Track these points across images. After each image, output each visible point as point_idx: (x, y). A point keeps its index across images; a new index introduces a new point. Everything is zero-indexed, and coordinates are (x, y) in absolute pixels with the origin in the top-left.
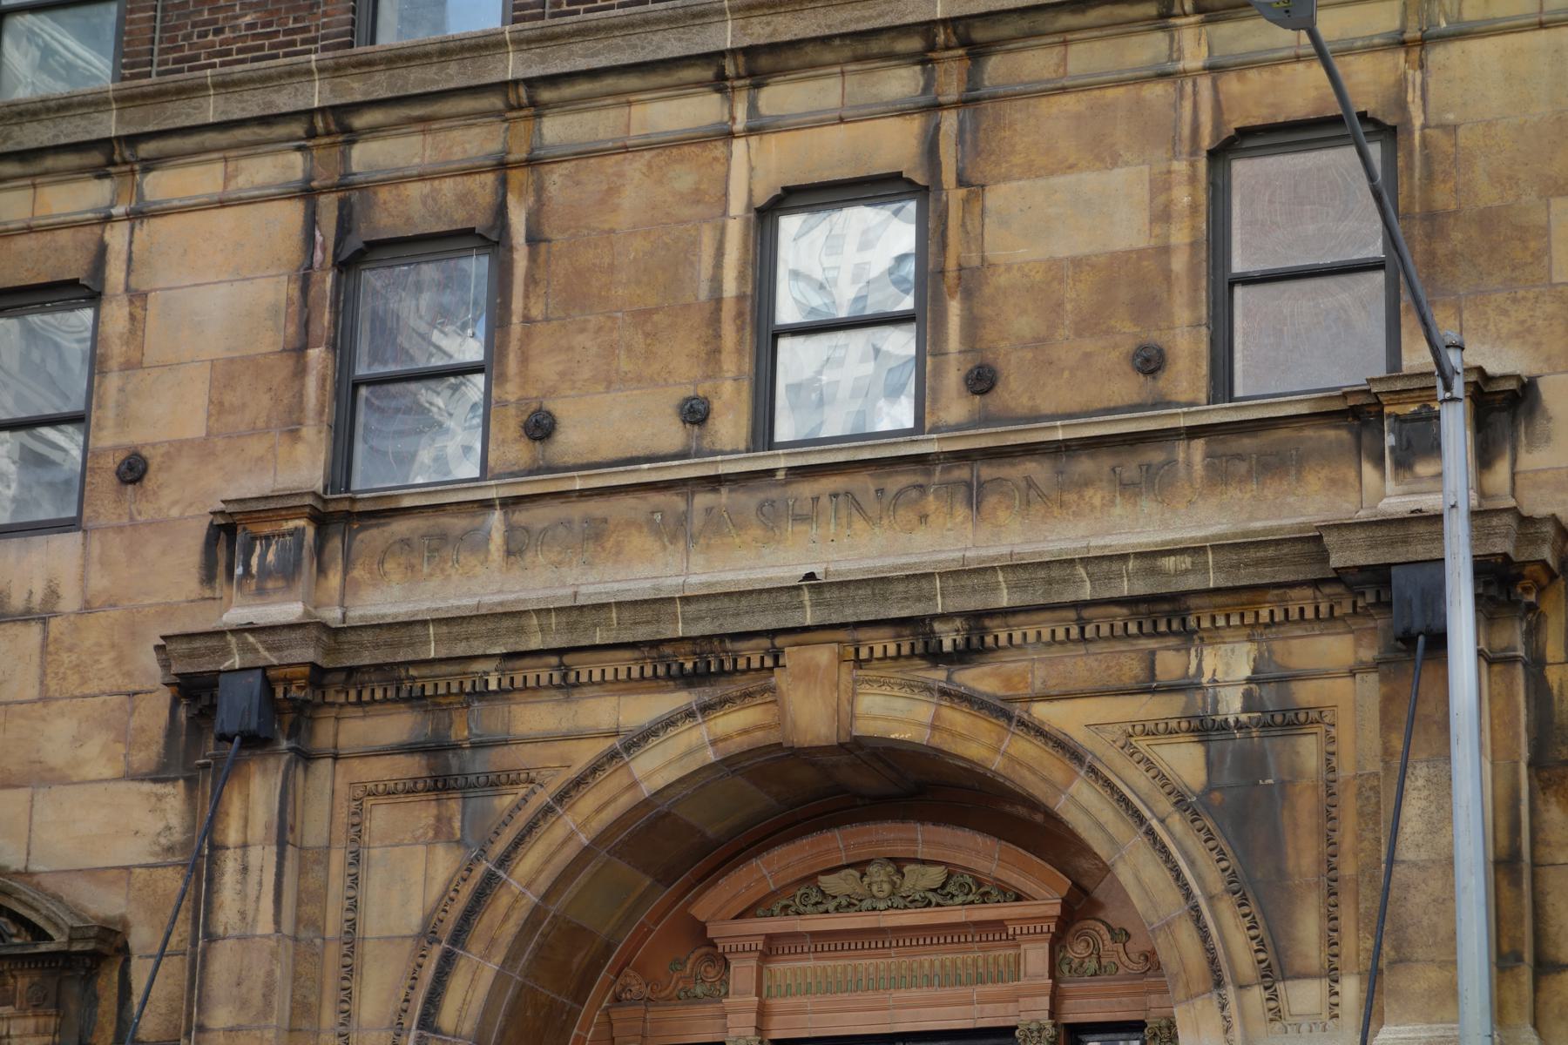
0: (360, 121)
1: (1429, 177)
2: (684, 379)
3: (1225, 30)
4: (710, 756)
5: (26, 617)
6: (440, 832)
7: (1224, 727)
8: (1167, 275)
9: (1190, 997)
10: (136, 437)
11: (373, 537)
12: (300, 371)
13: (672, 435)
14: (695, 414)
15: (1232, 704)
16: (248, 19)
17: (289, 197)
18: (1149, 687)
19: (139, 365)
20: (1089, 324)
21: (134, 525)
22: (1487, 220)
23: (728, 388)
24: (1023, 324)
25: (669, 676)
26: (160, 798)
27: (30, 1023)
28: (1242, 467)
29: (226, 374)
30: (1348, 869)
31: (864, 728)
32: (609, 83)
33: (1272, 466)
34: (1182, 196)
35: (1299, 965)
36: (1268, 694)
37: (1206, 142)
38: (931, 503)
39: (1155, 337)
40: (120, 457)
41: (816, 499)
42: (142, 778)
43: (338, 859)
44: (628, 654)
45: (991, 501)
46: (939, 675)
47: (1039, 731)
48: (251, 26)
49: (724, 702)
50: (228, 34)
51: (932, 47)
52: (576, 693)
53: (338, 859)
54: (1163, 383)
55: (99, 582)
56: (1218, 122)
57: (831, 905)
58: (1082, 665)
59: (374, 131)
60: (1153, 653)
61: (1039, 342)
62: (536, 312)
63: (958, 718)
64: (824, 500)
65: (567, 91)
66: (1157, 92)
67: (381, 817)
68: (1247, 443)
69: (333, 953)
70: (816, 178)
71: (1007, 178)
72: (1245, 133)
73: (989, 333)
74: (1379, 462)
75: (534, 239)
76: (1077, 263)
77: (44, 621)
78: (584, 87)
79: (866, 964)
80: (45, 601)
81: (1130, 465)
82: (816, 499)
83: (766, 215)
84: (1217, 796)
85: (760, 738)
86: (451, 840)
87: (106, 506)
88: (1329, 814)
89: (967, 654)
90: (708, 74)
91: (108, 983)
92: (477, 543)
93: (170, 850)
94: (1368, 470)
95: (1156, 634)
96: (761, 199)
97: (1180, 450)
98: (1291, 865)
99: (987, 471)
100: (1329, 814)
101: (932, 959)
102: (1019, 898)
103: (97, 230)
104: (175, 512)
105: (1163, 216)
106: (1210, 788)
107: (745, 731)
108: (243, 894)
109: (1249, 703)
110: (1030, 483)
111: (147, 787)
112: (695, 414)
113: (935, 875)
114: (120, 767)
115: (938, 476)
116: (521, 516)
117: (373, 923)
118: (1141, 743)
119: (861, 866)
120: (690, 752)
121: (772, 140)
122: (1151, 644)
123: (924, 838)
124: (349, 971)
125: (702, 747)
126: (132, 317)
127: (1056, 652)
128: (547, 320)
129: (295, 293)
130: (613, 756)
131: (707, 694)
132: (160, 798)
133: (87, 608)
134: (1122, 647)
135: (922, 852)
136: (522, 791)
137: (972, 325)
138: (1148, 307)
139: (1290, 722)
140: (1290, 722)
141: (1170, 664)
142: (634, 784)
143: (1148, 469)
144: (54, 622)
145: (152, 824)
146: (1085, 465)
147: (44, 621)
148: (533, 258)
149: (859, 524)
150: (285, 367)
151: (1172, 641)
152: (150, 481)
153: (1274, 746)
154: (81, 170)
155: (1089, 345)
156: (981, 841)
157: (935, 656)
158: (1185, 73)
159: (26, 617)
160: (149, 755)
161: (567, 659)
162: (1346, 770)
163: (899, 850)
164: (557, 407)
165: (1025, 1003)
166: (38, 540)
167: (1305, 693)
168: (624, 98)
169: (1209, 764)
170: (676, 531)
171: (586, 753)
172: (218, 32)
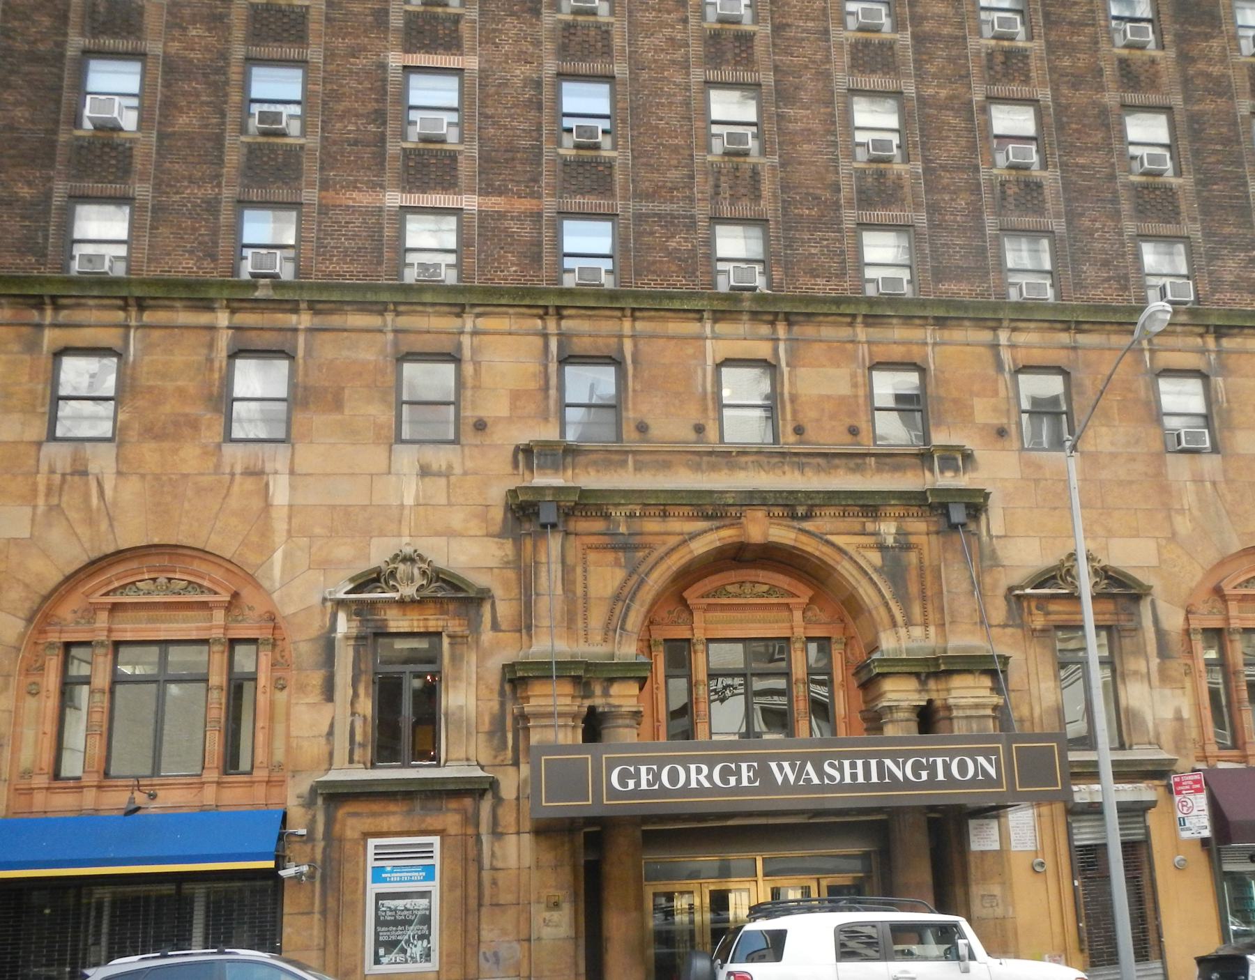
0: (565, 312)
1: (937, 385)
2: (694, 416)
3: (871, 330)
4: (718, 544)
5: (439, 474)
6: (617, 563)
7: (888, 547)
8: (858, 405)
9: (885, 630)
10: (482, 413)
11: (582, 459)
12: (547, 397)
13: (692, 436)
14: (699, 429)
15: (890, 541)
16: (514, 269)
17: (535, 334)
18: (863, 533)
19: (480, 387)
20: (833, 417)
21: (482, 445)
22: (956, 401)
23: (711, 422)
24: (813, 414)
25: (702, 516)
26: (502, 544)
27: (457, 622)
28: (887, 468)
29: (516, 396)
30: (929, 593)
31: (771, 539)
32: (662, 313)
33: (896, 468)
34: (860, 380)
35: (914, 622)
36: (901, 538)
37: (867, 364)
38: (786, 468)
39: (855, 423)
40: (475, 420)
41: (746, 463)
42: (494, 536)
43: (579, 570)
44: (689, 508)
45: (807, 469)
46: (795, 524)
47: (832, 545)
48: (515, 271)
49: (723, 527)
50: (506, 273)
51: (546, 314)
52: (667, 519)
53: (579, 570)
54: (859, 438)
55: (469, 464)
56: (871, 359)
57: (141, 593)
58: (842, 525)
59: (570, 317)
60: (864, 523)
61: (818, 421)
62: (638, 387)
63: (803, 538)
64: (750, 464)
65: (646, 314)
66: (849, 346)
67: (592, 556)
68: (888, 460)
69: (580, 602)
70: (736, 357)
71: (804, 366)
72: (878, 363)
73: (800, 416)
74: (932, 470)
75: (635, 361)
76: (829, 397)
77: (448, 476)
78: (652, 313)
79: (738, 615)
80: (447, 468)
81: (852, 463)
82: (746, 463)
83: (719, 366)
84: (885, 569)
85: (736, 539)
86: (620, 566)
87: (469, 437)
88: (921, 576)
89: (808, 517)
90: (697, 316)
91: (486, 609)
92: (623, 464)
93: (508, 563)
94: (928, 474)
95: (867, 516)
96: (718, 361)
97: (867, 460)
98: (910, 590)
99: (804, 460)
100: (921, 576)
101: (760, 614)
102: (216, 593)
103: (457, 336)
104: (499, 442)
105: (855, 385)
106: (883, 566)
107: (730, 537)
108: (549, 580)
109: (896, 541)
110: (819, 465)
111: (496, 540)
112: (699, 429)
113: (765, 588)
114: (484, 532)
115: (788, 459)
116: (639, 457)
117: (593, 592)
118: (861, 550)
119: (742, 583)
120: (711, 542)
121: (720, 342)
122: (864, 520)
123: (762, 575)
124: (586, 610)
125: (715, 541)
126: (475, 370)
127: (834, 519)
128: (642, 391)
129: (542, 368)
130: (685, 541)
131: (716, 523)
132: (502, 544)
133: (465, 473)
134: (854, 519)
135: (761, 580)
136: (647, 551)
137: (794, 412)
138: (853, 414)
139: (907, 547)
140: (907, 547)
141: (870, 527)
142: (691, 552)
143: (857, 465)
144: (451, 477)
145: (499, 553)
146: (837, 461)
147: (448, 476)
148: (635, 369)
149: (762, 473)
150: (540, 396)
151: (871, 519)
152: (488, 430)
153: (904, 554)
154: (450, 313)
155: (834, 423)
156: (781, 577)
157: (794, 517)
158: (859, 342)
159: (439, 474)
160: (496, 528)
161: (667, 508)
162: (926, 562)
163: (753, 579)
164: (649, 421)
165: (214, 631)
166: (442, 446)
167: (913, 539)
168: (665, 319)
169: (883, 558)
170: (697, 468)
171: (673, 541)
172: (502, 271)
